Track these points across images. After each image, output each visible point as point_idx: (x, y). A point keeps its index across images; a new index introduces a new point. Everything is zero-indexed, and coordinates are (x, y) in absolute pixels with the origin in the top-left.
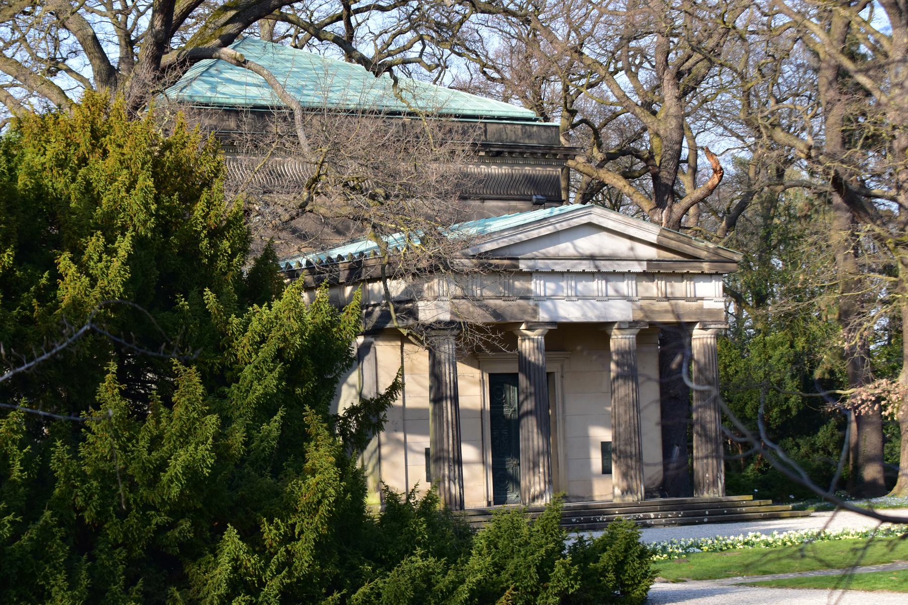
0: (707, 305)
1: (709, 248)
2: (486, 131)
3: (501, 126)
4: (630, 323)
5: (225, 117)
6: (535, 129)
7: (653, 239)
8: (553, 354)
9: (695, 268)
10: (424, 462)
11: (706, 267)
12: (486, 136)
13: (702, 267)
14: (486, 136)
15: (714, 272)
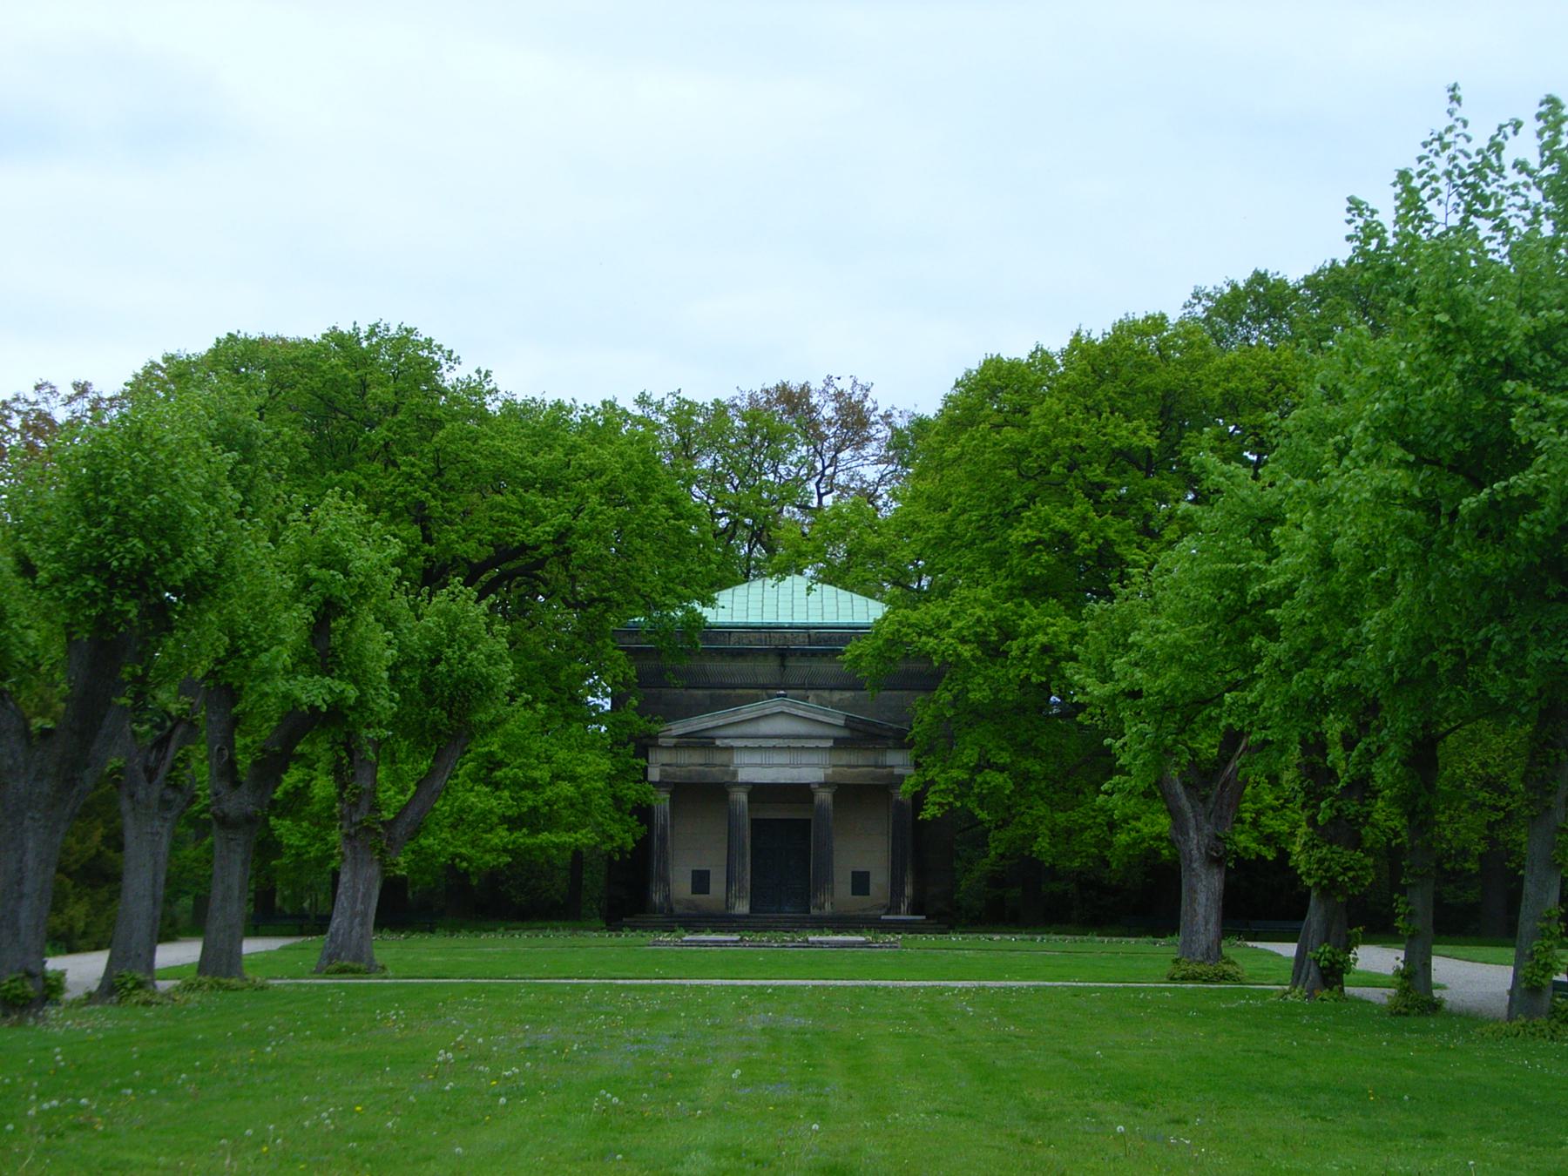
7: (841, 722)
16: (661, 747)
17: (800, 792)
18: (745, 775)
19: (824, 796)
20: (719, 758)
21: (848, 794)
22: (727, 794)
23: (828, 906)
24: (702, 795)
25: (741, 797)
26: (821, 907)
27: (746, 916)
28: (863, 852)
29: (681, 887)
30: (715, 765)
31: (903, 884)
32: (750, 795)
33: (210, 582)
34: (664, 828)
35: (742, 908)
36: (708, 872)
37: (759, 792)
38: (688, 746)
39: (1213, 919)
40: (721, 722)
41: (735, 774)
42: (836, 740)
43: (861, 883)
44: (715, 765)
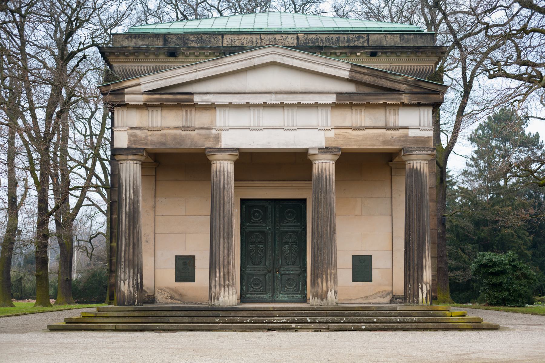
0: (412, 133)
1: (409, 81)
2: (368, 40)
3: (382, 36)
4: (319, 149)
5: (155, 39)
6: (412, 36)
7: (345, 74)
8: (240, 183)
9: (393, 99)
10: (144, 282)
11: (405, 98)
12: (368, 43)
13: (401, 99)
14: (368, 43)
15: (416, 102)
16: (126, 105)
17: (295, 163)
18: (229, 140)
19: (325, 165)
20: (200, 119)
21: (361, 166)
22: (208, 165)
23: (331, 295)
24: (177, 166)
25: (225, 167)
26: (323, 296)
27: (233, 309)
28: (369, 235)
29: (158, 273)
30: (195, 129)
31: (420, 268)
32: (237, 164)
33: (268, 5)
34: (135, 204)
35: (229, 297)
36: (193, 257)
37: (252, 163)
38: (162, 106)
39: (497, 357)
40: (200, 75)
41: (217, 138)
42: (339, 94)
43: (362, 268)
44: (195, 129)
